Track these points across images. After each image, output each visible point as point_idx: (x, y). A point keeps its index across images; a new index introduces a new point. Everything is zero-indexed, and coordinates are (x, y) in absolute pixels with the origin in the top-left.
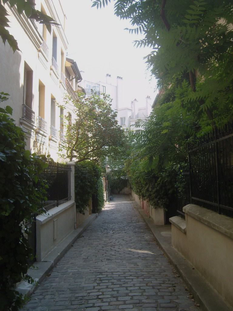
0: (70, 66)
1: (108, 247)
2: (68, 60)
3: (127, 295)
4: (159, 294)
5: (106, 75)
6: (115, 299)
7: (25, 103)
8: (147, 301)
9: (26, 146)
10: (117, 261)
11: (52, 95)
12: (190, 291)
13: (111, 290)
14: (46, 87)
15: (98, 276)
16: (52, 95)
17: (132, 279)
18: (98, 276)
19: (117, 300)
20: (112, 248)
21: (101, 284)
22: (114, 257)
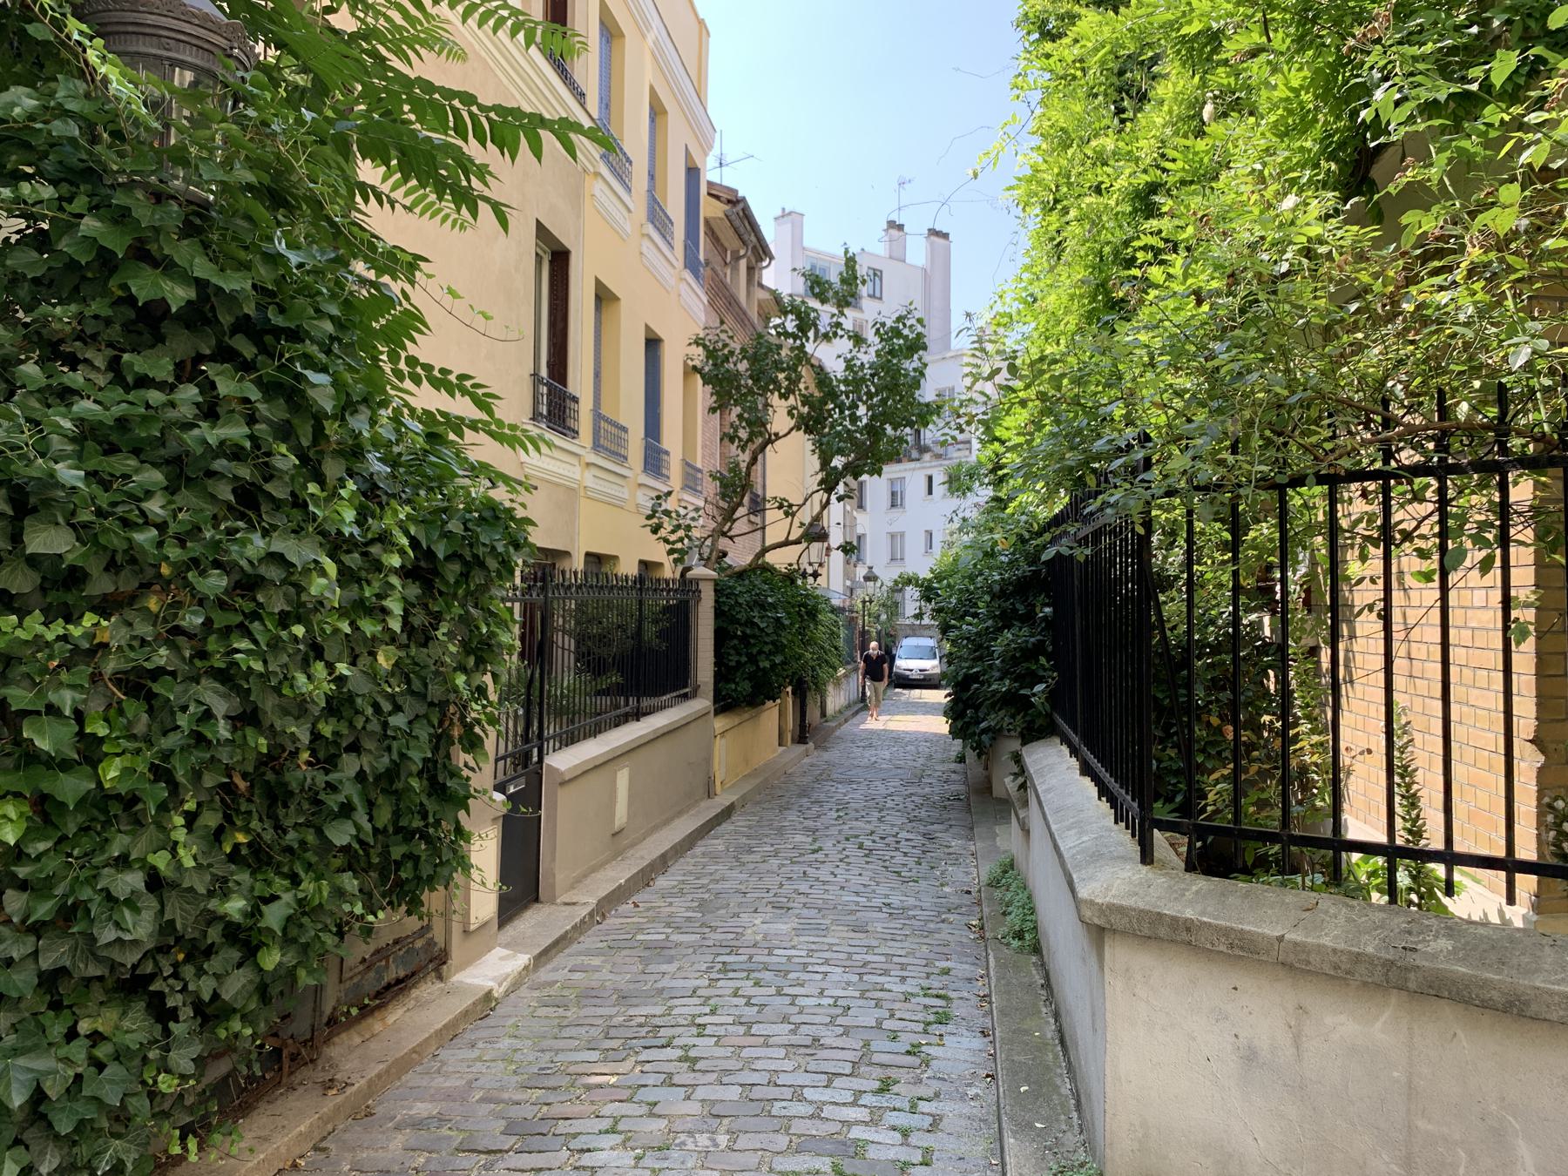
0: (721, 215)
1: (796, 868)
2: (716, 192)
3: (785, 1019)
4: (887, 1024)
5: (885, 226)
6: (742, 1030)
7: (544, 373)
8: (839, 1042)
9: (530, 529)
10: (805, 912)
11: (647, 328)
12: (399, 981)
13: (743, 1001)
14: (624, 304)
15: (720, 959)
16: (647, 328)
17: (826, 974)
18: (720, 959)
19: (748, 1034)
20: (809, 870)
21: (720, 983)
22: (803, 899)
